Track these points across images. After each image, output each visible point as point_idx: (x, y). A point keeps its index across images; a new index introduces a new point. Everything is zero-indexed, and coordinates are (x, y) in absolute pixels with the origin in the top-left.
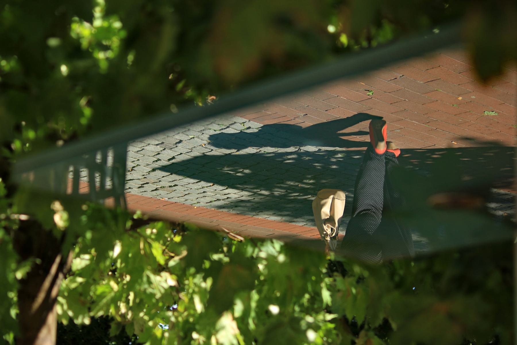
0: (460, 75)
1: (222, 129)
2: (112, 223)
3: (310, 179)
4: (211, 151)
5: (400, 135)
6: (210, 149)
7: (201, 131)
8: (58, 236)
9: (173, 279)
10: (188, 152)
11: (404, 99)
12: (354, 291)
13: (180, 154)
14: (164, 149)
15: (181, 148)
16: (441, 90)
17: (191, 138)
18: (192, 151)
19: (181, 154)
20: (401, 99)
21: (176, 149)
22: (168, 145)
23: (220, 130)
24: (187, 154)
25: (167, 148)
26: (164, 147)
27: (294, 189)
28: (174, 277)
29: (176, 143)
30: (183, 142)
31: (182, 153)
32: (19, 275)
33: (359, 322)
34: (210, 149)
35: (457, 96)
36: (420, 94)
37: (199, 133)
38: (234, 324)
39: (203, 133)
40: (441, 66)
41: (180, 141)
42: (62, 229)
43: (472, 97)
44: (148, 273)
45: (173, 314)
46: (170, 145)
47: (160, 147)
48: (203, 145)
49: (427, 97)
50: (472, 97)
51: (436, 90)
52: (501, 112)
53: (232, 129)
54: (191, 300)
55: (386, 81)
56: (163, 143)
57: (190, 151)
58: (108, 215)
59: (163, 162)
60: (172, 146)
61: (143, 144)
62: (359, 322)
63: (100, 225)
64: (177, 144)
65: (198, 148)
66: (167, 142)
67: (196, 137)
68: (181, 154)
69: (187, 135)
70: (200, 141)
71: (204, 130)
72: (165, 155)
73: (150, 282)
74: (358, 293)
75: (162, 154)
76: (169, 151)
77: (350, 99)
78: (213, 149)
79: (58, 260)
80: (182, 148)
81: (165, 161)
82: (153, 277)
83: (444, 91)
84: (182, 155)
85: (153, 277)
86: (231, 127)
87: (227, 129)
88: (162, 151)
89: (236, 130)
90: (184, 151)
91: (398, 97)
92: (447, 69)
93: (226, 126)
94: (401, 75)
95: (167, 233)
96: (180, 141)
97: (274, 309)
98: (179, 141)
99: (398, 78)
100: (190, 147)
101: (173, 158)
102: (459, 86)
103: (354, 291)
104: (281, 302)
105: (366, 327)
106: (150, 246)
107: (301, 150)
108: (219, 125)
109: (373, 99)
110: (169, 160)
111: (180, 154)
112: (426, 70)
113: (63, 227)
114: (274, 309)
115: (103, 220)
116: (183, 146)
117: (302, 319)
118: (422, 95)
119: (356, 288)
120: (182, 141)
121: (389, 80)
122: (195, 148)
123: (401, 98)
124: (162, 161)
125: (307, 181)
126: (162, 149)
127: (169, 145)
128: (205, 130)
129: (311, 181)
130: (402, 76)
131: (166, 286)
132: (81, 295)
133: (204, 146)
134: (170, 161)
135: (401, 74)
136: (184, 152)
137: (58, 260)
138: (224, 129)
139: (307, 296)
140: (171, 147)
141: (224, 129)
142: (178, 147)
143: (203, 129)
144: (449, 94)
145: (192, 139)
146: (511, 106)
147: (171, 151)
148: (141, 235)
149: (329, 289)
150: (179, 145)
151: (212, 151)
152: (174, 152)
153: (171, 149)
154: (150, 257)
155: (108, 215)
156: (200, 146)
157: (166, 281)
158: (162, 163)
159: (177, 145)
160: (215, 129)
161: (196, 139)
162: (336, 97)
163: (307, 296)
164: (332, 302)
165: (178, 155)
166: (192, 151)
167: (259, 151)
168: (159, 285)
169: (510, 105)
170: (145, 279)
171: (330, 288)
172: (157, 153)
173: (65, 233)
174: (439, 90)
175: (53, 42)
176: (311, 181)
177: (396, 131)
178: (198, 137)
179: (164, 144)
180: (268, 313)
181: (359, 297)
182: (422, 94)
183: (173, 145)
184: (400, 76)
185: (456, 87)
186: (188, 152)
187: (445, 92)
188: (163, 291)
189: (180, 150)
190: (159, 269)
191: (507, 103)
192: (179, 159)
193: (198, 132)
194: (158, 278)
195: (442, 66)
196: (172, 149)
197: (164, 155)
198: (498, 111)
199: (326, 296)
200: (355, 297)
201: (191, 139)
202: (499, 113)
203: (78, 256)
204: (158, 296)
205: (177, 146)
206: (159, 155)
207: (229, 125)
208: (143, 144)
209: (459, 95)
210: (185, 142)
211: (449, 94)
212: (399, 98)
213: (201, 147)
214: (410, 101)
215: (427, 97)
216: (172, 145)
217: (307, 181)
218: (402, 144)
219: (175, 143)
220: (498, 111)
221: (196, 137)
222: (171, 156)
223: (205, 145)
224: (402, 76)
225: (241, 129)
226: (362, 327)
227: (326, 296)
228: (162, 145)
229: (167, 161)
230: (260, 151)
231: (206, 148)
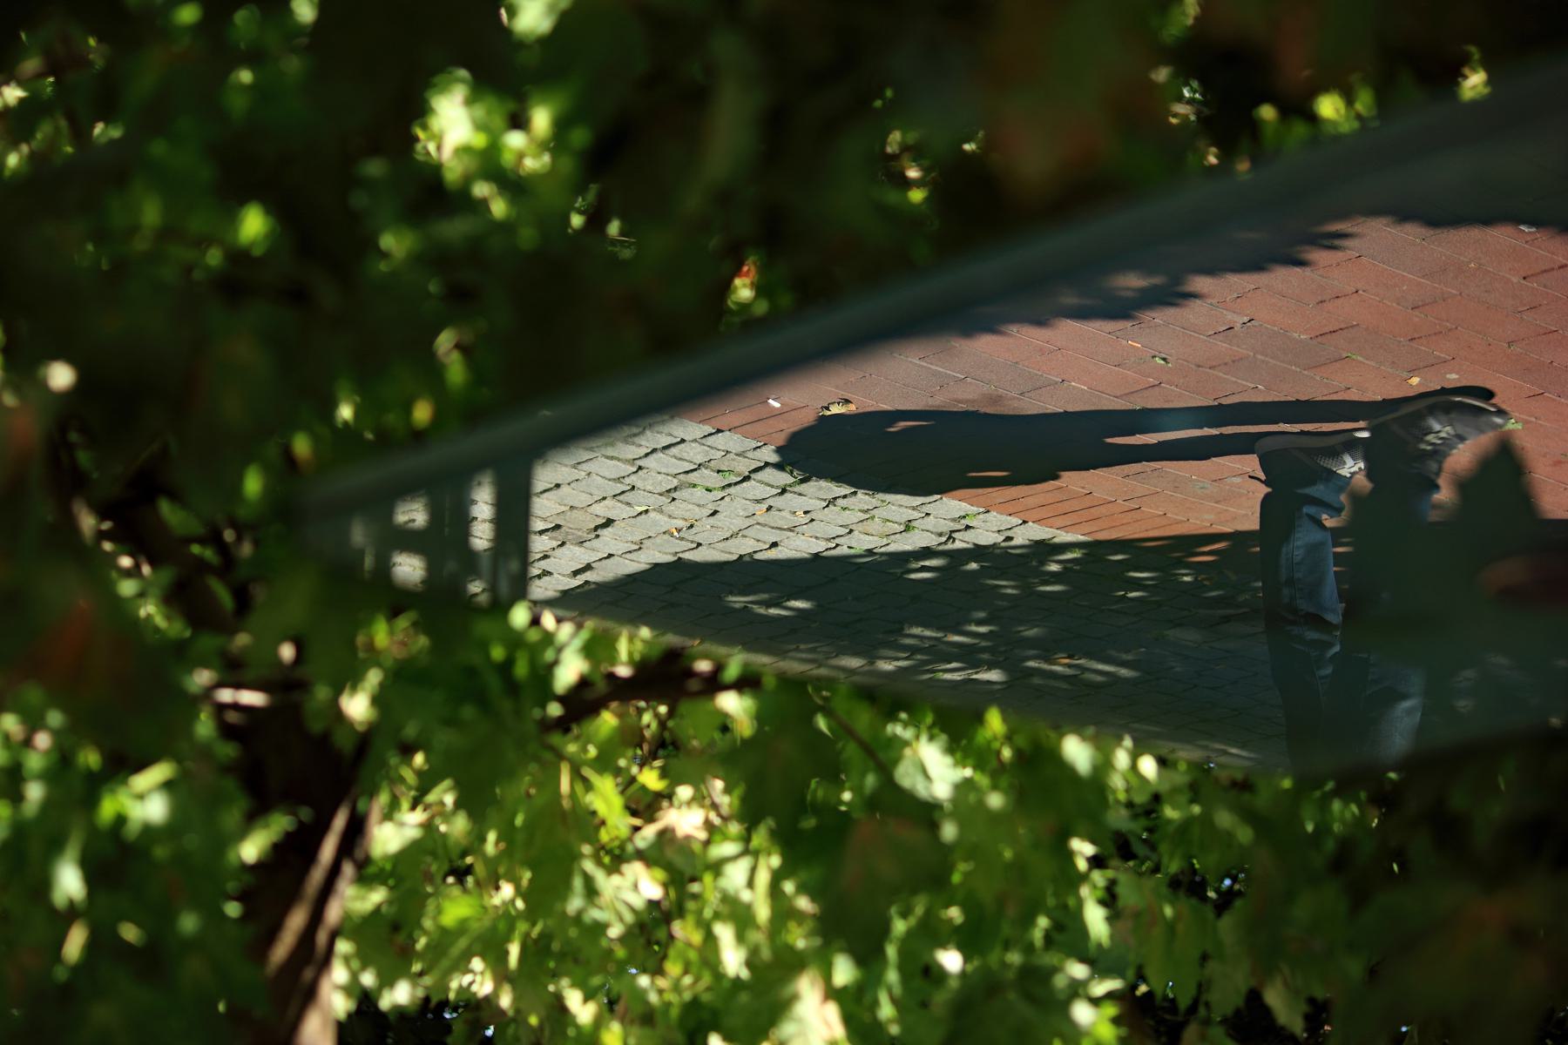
0: (1416, 312)
1: (729, 485)
2: (506, 705)
3: (980, 623)
4: (697, 547)
5: (1242, 491)
6: (692, 542)
7: (669, 491)
8: (345, 743)
9: (654, 878)
10: (630, 552)
11: (1253, 386)
12: (1168, 911)
13: (605, 558)
14: (563, 544)
15: (609, 541)
16: (1362, 356)
17: (641, 513)
18: (640, 548)
19: (610, 556)
20: (1244, 386)
21: (595, 543)
22: (573, 534)
23: (723, 488)
24: (628, 556)
25: (569, 540)
26: (560, 538)
27: (942, 654)
28: (660, 874)
29: (596, 528)
30: (616, 523)
31: (613, 555)
32: (251, 850)
33: (1184, 1003)
34: (692, 542)
35: (1405, 374)
36: (1298, 370)
37: (664, 498)
38: (832, 1011)
39: (674, 499)
40: (1360, 292)
41: (609, 523)
42: (360, 728)
43: (1448, 376)
44: (589, 866)
45: (653, 982)
46: (580, 533)
47: (550, 538)
48: (674, 531)
49: (1318, 378)
50: (1448, 376)
51: (1344, 355)
52: (1534, 420)
53: (758, 484)
54: (710, 938)
55: (1202, 336)
56: (558, 527)
57: (637, 547)
58: (494, 683)
59: (557, 580)
60: (585, 535)
61: (631, 451)
62: (1184, 1003)
63: (468, 712)
64: (599, 530)
65: (658, 540)
66: (571, 526)
67: (654, 510)
68: (610, 556)
69: (628, 504)
70: (666, 519)
71: (675, 489)
72: (562, 561)
73: (591, 891)
74: (1178, 917)
75: (555, 558)
76: (577, 548)
77: (1097, 389)
78: (700, 542)
79: (340, 821)
80: (614, 541)
81: (564, 575)
82: (599, 876)
83: (1367, 359)
84: (612, 559)
85: (599, 876)
86: (754, 480)
87: (745, 484)
88: (556, 551)
89: (769, 485)
90: (618, 547)
91: (1234, 379)
92: (1378, 299)
93: (740, 475)
94: (1246, 319)
95: (624, 756)
96: (609, 523)
97: (951, 960)
98: (604, 521)
99: (1238, 327)
100: (637, 539)
101: (588, 567)
102: (1411, 344)
103: (1168, 911)
104: (967, 941)
105: (1202, 1011)
106: (588, 786)
107: (954, 541)
108: (720, 473)
109: (1165, 388)
110: (576, 573)
111: (605, 558)
112: (1318, 303)
113: (361, 723)
114: (951, 960)
115: (482, 700)
116: (615, 534)
117: (1056, 970)
118: (1306, 372)
119: (1172, 904)
120: (613, 521)
121: (1210, 333)
122: (650, 540)
123: (1244, 383)
124: (555, 575)
125: (974, 628)
126: (555, 544)
127: (576, 532)
128: (681, 489)
129: (983, 629)
130: (1250, 321)
131: (638, 902)
132: (396, 927)
133: (676, 534)
134: (578, 577)
135: (1247, 316)
136: (618, 550)
137: (340, 821)
138: (736, 484)
139: (1043, 922)
140: (580, 537)
141: (736, 484)
142: (601, 538)
143: (673, 487)
144: (1382, 367)
145: (643, 516)
146: (1563, 400)
147: (582, 550)
148: (560, 756)
149: (1102, 902)
150: (604, 532)
151: (700, 548)
152: (591, 551)
153: (582, 542)
154: (590, 823)
155: (494, 683)
156: (664, 533)
157: (635, 887)
158: (554, 582)
159: (599, 532)
160: (710, 485)
161: (652, 515)
162: (1056, 383)
163: (1043, 922)
164: (1112, 937)
165: (600, 560)
166: (640, 548)
167: (834, 545)
168: (617, 899)
169: (1558, 398)
170: (578, 883)
171: (1109, 899)
172: (542, 555)
173: (366, 740)
174: (1354, 357)
175: (374, 168)
176: (983, 629)
177: (1228, 481)
178: (660, 510)
179: (563, 530)
180: (934, 974)
181: (1180, 928)
182: (1305, 370)
183: (588, 534)
184: (1241, 322)
185: (1404, 346)
186: (630, 552)
187: (1373, 364)
188: (629, 918)
189: (607, 547)
190: (616, 859)
191: (1550, 393)
192: (604, 574)
193: (661, 495)
194: (616, 879)
195: (1364, 291)
196: (585, 544)
197: (560, 559)
198: (1522, 416)
199: (1095, 919)
200: (1171, 927)
201: (638, 515)
202: (1526, 422)
203: (389, 815)
204: (615, 932)
205: (598, 536)
206: (548, 560)
207: (750, 472)
208: (633, 448)
209: (1413, 371)
210: (623, 525)
211: (1382, 367)
212: (1239, 381)
213: (666, 537)
214: (1270, 390)
215: (1318, 378)
216: (583, 532)
217: (974, 628)
218: (1246, 515)
219: (593, 526)
220: (1522, 416)
221: (654, 510)
222: (582, 561)
223: (679, 531)
224: (1250, 321)
225: (785, 482)
226: (1193, 1009)
227: (1095, 919)
228: (555, 534)
229: (568, 576)
230: (837, 545)
231: (682, 539)
